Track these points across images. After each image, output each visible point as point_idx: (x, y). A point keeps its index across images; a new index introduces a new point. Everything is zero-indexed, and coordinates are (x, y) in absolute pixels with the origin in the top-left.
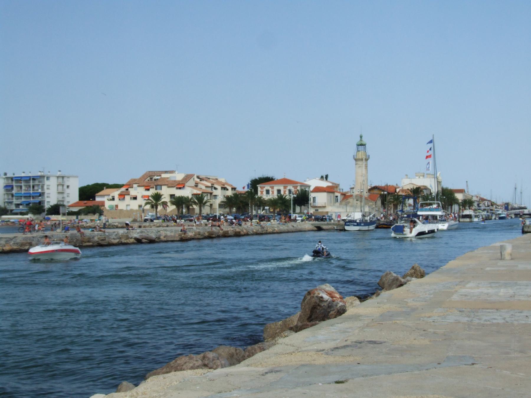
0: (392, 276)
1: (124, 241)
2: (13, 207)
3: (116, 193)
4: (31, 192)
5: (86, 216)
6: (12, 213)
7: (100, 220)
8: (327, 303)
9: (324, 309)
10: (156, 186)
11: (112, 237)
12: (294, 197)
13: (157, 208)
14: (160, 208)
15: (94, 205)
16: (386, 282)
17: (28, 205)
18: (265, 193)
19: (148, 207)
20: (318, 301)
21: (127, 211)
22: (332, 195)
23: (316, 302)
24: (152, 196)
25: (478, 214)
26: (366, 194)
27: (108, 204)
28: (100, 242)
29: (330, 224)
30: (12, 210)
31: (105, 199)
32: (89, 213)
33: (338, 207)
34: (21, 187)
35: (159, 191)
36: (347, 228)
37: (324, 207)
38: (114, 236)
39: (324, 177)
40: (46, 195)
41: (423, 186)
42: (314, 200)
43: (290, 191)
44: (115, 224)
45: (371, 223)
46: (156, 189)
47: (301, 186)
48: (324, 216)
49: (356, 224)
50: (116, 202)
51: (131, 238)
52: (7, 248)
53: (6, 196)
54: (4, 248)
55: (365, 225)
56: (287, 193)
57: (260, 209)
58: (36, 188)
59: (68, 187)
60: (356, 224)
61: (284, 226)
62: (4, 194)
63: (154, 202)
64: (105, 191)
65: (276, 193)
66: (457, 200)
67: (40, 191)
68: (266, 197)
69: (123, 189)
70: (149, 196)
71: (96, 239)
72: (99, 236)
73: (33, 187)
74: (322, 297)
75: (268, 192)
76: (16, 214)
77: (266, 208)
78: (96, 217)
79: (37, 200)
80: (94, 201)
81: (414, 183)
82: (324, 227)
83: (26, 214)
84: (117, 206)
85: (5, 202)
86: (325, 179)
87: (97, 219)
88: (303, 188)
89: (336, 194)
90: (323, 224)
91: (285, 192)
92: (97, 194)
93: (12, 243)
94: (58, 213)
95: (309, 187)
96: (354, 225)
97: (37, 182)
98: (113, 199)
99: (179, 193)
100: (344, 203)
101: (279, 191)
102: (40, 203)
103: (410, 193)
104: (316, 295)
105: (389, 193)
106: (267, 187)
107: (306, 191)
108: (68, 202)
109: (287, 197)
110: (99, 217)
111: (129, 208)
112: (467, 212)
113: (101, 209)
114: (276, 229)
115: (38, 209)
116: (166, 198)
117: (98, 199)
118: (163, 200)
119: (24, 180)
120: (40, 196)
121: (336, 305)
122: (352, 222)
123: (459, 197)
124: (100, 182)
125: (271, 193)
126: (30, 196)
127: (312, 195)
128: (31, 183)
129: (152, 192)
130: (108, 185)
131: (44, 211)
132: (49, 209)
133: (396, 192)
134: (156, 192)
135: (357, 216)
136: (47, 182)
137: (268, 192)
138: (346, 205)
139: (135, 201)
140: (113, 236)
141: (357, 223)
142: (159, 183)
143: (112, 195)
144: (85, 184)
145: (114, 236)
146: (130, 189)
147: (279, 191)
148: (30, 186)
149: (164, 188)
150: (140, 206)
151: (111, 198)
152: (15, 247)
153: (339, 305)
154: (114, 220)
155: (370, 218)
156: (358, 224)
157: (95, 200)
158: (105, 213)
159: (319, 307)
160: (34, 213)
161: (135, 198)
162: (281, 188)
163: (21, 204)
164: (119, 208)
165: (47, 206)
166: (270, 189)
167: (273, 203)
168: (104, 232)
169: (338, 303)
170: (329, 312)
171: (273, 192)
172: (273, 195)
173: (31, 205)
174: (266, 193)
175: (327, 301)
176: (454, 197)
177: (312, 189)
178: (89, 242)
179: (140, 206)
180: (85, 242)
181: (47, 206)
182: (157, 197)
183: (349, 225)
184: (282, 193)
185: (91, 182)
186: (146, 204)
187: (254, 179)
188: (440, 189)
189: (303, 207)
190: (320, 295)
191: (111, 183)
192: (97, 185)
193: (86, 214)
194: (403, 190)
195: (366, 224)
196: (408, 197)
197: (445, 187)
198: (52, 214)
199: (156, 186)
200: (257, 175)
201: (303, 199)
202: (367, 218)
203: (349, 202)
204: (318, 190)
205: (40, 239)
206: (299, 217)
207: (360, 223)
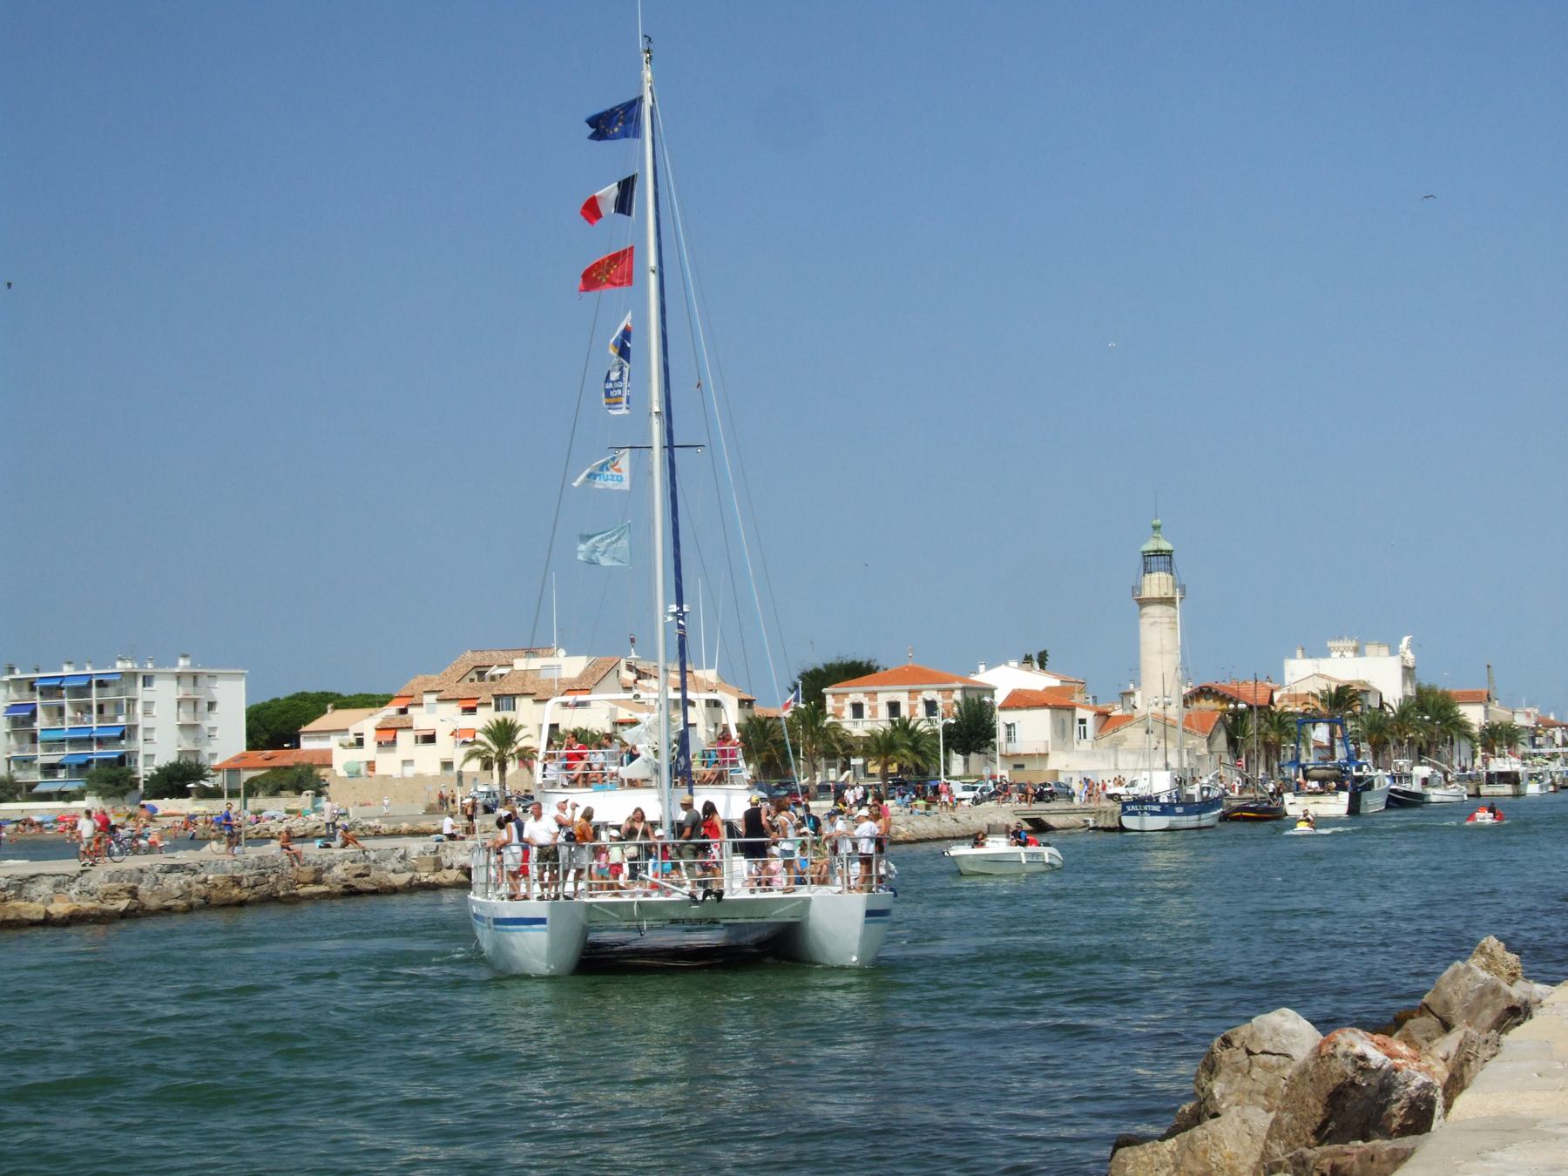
0: (1476, 979)
1: (425, 876)
2: (35, 776)
3: (367, 722)
4: (95, 724)
5: (273, 800)
6: (30, 792)
7: (315, 810)
8: (1381, 1074)
9: (1367, 1097)
10: (497, 697)
11: (390, 867)
12: (946, 727)
13: (503, 768)
14: (512, 767)
15: (297, 765)
16: (1455, 1000)
17: (83, 767)
18: (848, 713)
19: (475, 765)
20: (1349, 1070)
21: (403, 779)
22: (1067, 715)
23: (1344, 1075)
24: (488, 732)
25: (1538, 769)
26: (1174, 712)
27: (343, 760)
28: (354, 882)
29: (1074, 811)
30: (31, 786)
31: (333, 743)
32: (282, 788)
33: (1087, 755)
34: (61, 710)
35: (509, 715)
36: (1128, 822)
37: (1044, 756)
38: (393, 860)
39: (1035, 657)
40: (140, 735)
41: (1358, 682)
42: (1009, 734)
43: (931, 707)
44: (372, 824)
45: (1207, 804)
46: (497, 709)
47: (964, 690)
48: (1045, 785)
49: (1157, 808)
50: (370, 751)
51: (450, 868)
52: (60, 908)
53: (13, 741)
54: (52, 909)
55: (1186, 813)
56: (921, 711)
57: (834, 766)
58: (108, 712)
59: (211, 705)
60: (1157, 808)
61: (926, 820)
62: (8, 734)
63: (496, 749)
64: (332, 718)
65: (883, 712)
66: (1467, 726)
67: (122, 720)
68: (859, 729)
69: (391, 710)
70: (473, 732)
71: (338, 871)
72: (347, 864)
73: (101, 709)
74: (1363, 1057)
75: (858, 710)
76: (47, 797)
77: (853, 762)
78: (304, 801)
79: (112, 752)
80: (295, 751)
81: (1329, 674)
82: (1052, 821)
83: (79, 796)
84: (371, 765)
85: (9, 760)
86: (1036, 665)
87: (308, 808)
88: (972, 695)
89: (1080, 713)
90: (1049, 812)
91: (912, 708)
92: (304, 729)
93: (75, 888)
94: (184, 793)
95: (991, 691)
96: (1153, 813)
97: (110, 694)
98: (360, 743)
99: (571, 721)
100: (1105, 742)
101: (894, 708)
102: (122, 760)
103: (1319, 705)
104: (1340, 1050)
105: (1251, 707)
106: (857, 693)
107: (982, 704)
108: (213, 756)
109: (923, 727)
110: (314, 803)
111: (409, 772)
112: (1497, 765)
113: (318, 777)
114: (903, 829)
115: (114, 778)
116: (532, 737)
117: (306, 745)
118: (522, 744)
119: (70, 689)
120: (122, 737)
121: (1406, 1084)
122: (1143, 803)
123: (1474, 715)
124: (313, 688)
125: (867, 712)
126: (90, 739)
127: (1002, 718)
128: (94, 697)
129: (486, 717)
130: (339, 696)
131: (134, 784)
132: (153, 777)
133: (1271, 702)
134: (500, 716)
135: (1160, 784)
136: (141, 693)
137: (858, 710)
138: (1115, 746)
139: (429, 747)
140: (392, 863)
141: (1163, 805)
142: (508, 690)
143: (354, 729)
144: (264, 698)
145: (393, 860)
146: (411, 710)
147: (894, 708)
148: (89, 707)
149: (524, 704)
150: (447, 765)
151: (353, 739)
152: (87, 905)
153: (1415, 1083)
154: (366, 811)
155: (1202, 789)
156: (1166, 810)
157: (298, 746)
158: (330, 790)
159: (1352, 1091)
160: (103, 794)
161: (430, 739)
162: (903, 698)
163: (63, 767)
164: (380, 770)
165: (143, 770)
166: (865, 700)
167: (881, 747)
168: (807, 808)
169: (1411, 1077)
170: (1384, 1107)
171: (874, 710)
172: (876, 721)
173: (93, 766)
174: (859, 713)
175: (1379, 1069)
176: (1457, 715)
177: (999, 698)
178: (317, 882)
179: (447, 765)
180: (306, 884)
181: (143, 770)
182: (504, 734)
183: (1134, 813)
184: (904, 711)
185: (284, 691)
186: (470, 756)
187: (810, 669)
188: (1411, 692)
189: (973, 756)
190: (1357, 1050)
191: (347, 691)
192: (303, 696)
193: (275, 792)
194: (1295, 698)
195: (1190, 807)
196: (1313, 719)
197: (1425, 684)
198: (159, 795)
199: (497, 697)
200: (818, 659)
201: (973, 730)
202: (1194, 790)
203: (1124, 739)
204: (1020, 701)
205: (161, 876)
206: (965, 789)
207: (1172, 805)
